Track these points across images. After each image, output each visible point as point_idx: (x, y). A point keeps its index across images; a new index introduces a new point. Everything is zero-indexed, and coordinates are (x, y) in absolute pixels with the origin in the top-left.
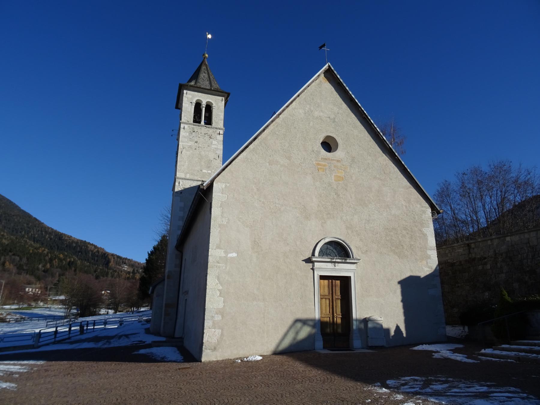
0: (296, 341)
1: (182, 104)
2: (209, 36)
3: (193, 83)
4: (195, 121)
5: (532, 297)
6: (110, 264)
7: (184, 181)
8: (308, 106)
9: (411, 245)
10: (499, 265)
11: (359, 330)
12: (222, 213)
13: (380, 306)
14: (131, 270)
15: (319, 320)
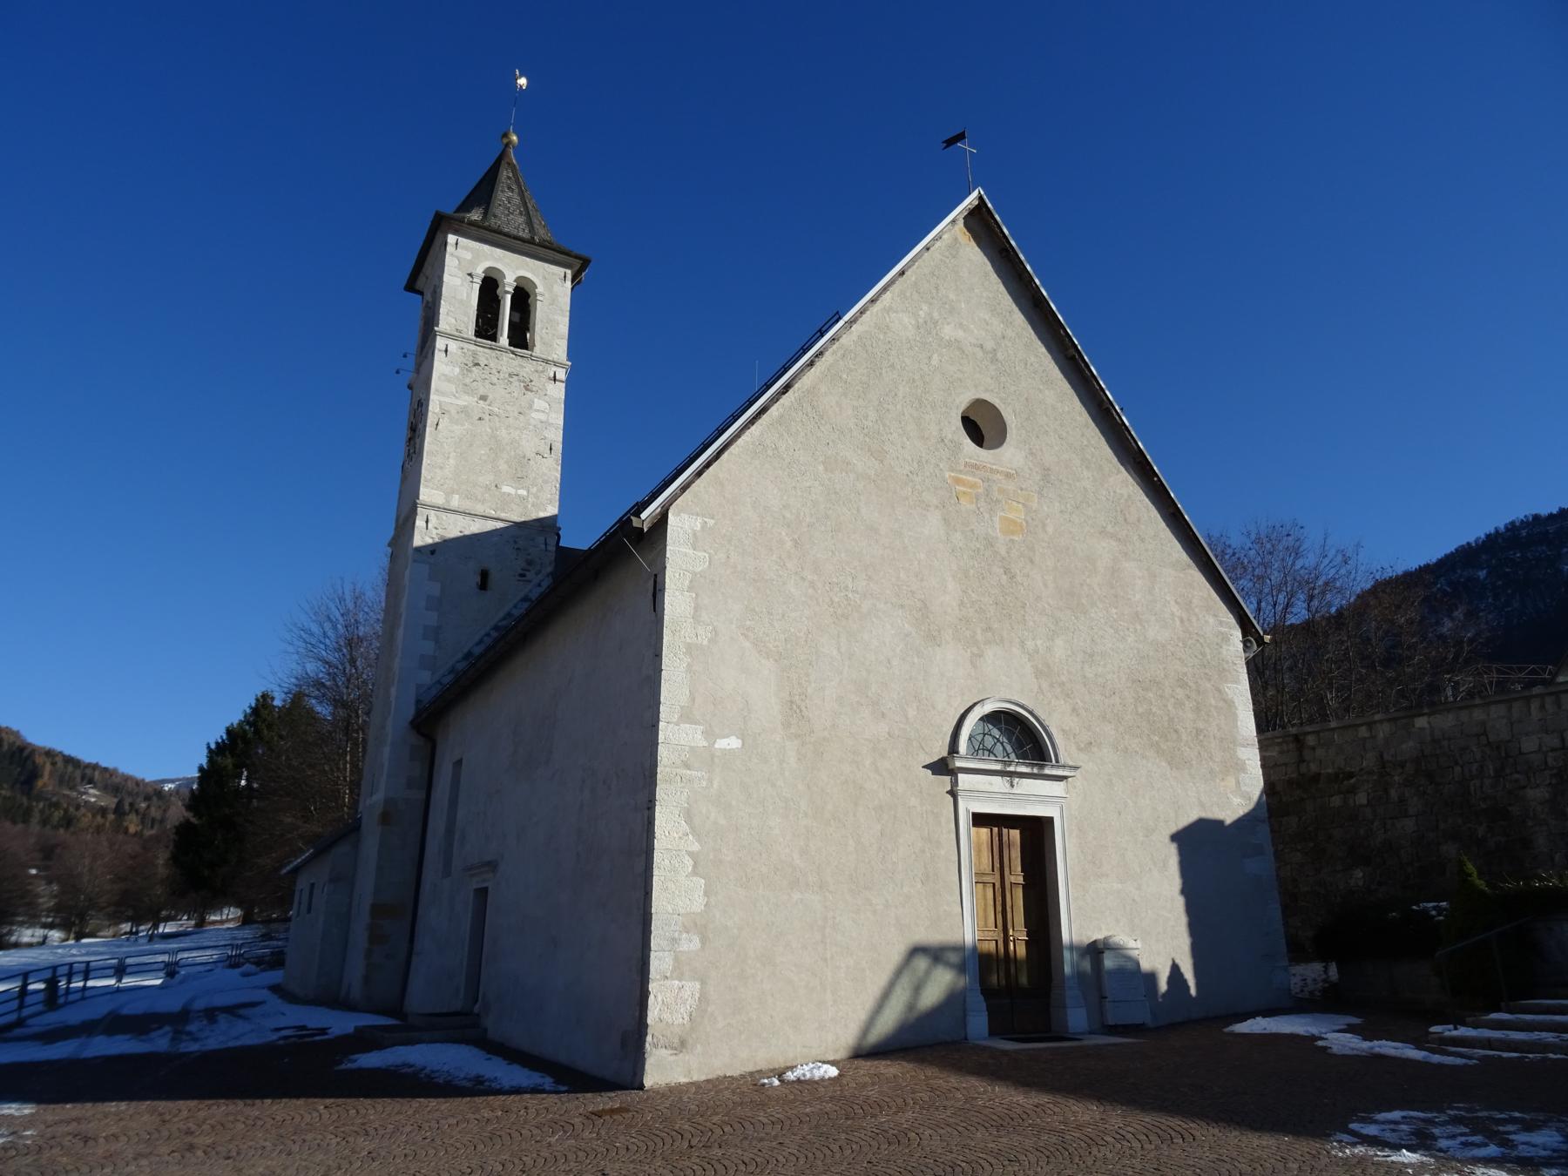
0: (915, 1014)
2: (523, 81)
3: (475, 215)
4: (478, 334)
5: (1541, 879)
6: (40, 783)
7: (444, 516)
8: (925, 307)
9: (1198, 731)
10: (1393, 793)
11: (1079, 975)
12: (696, 608)
13: (1130, 910)
14: (109, 802)
15: (975, 948)
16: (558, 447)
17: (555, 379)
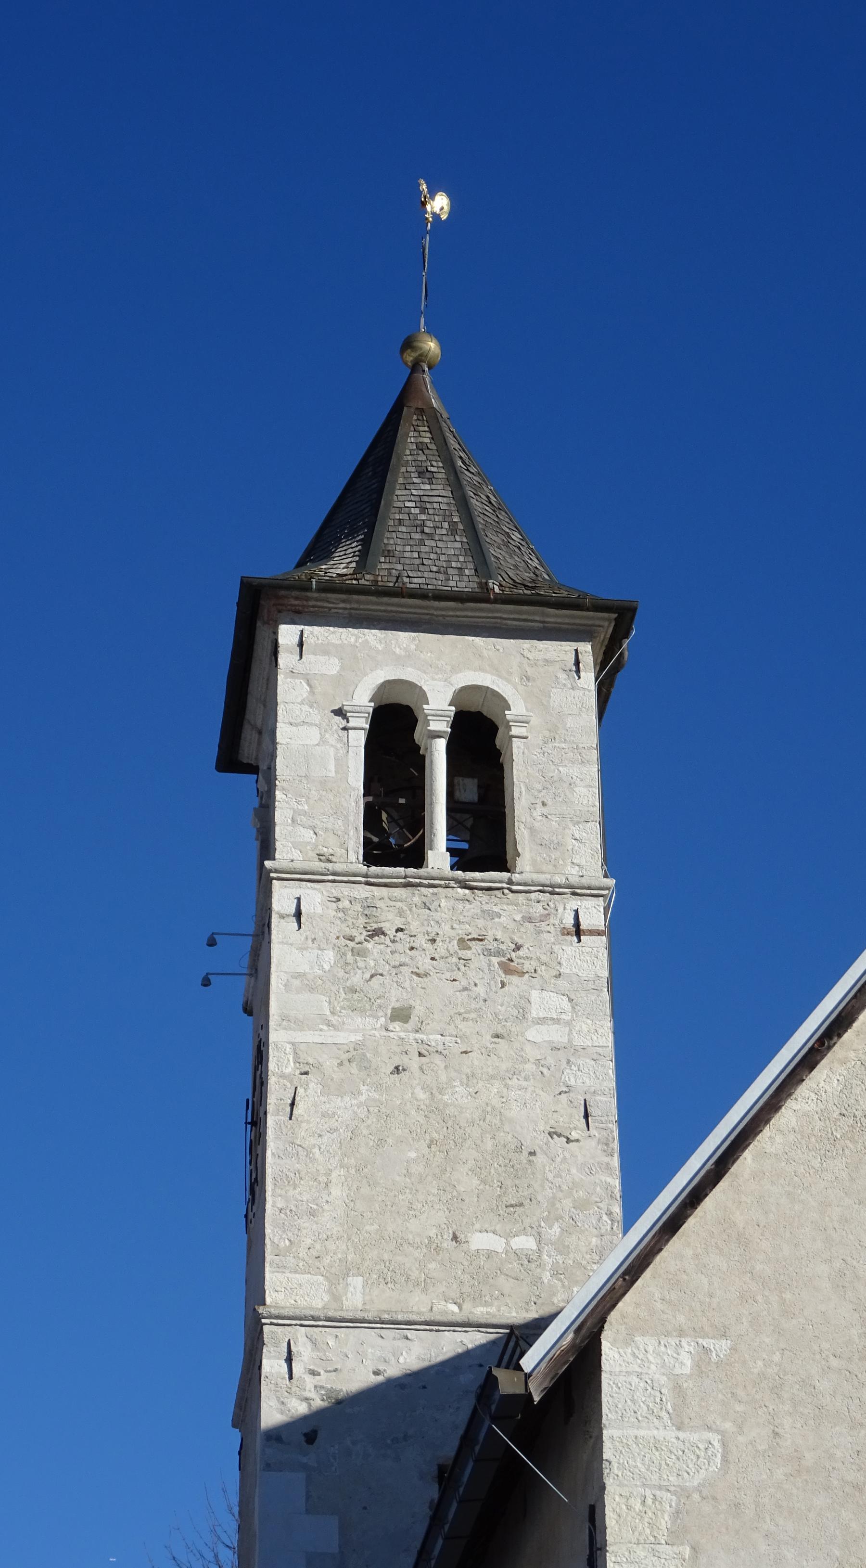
1: (267, 732)
2: (440, 204)
3: (340, 565)
4: (375, 853)
7: (328, 1336)
16: (606, 1106)
17: (578, 931)
